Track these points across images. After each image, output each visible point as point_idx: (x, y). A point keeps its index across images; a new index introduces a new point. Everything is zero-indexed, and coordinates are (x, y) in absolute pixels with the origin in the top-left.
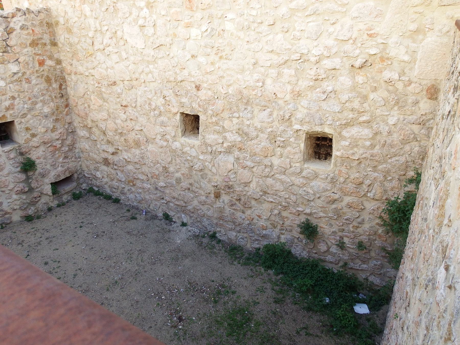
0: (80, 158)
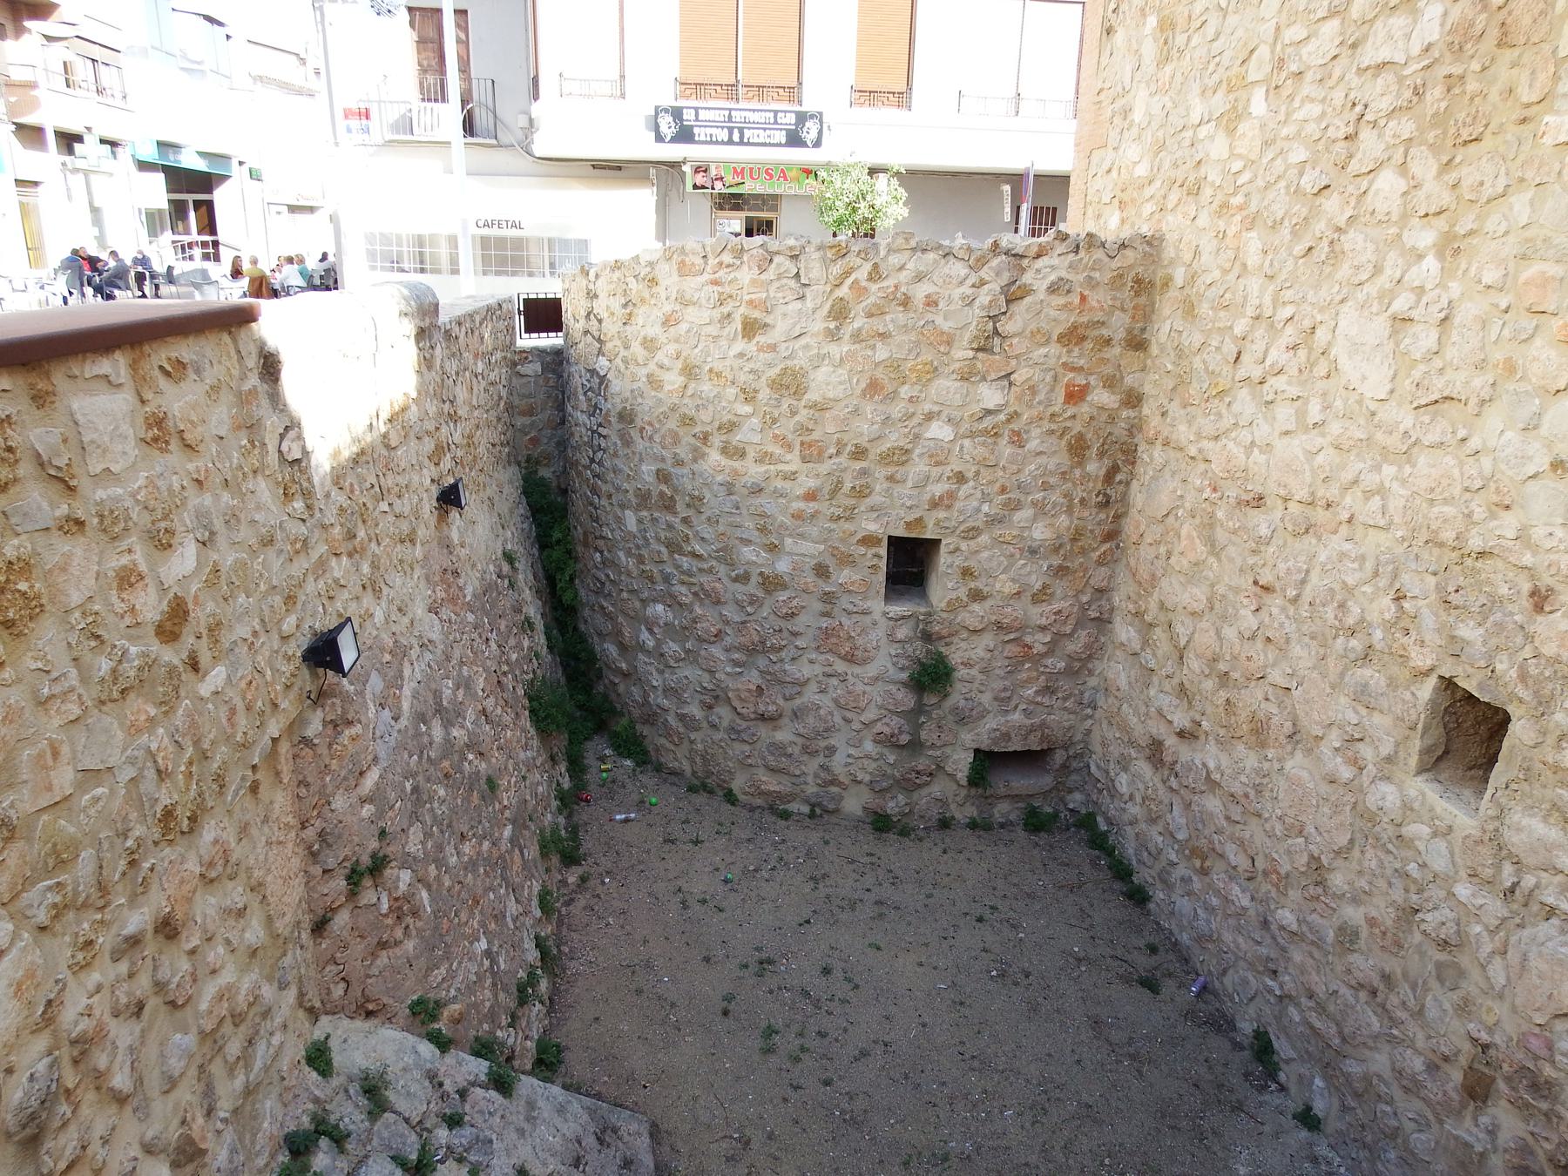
0: (1095, 708)
